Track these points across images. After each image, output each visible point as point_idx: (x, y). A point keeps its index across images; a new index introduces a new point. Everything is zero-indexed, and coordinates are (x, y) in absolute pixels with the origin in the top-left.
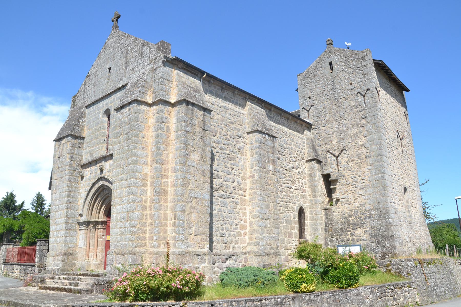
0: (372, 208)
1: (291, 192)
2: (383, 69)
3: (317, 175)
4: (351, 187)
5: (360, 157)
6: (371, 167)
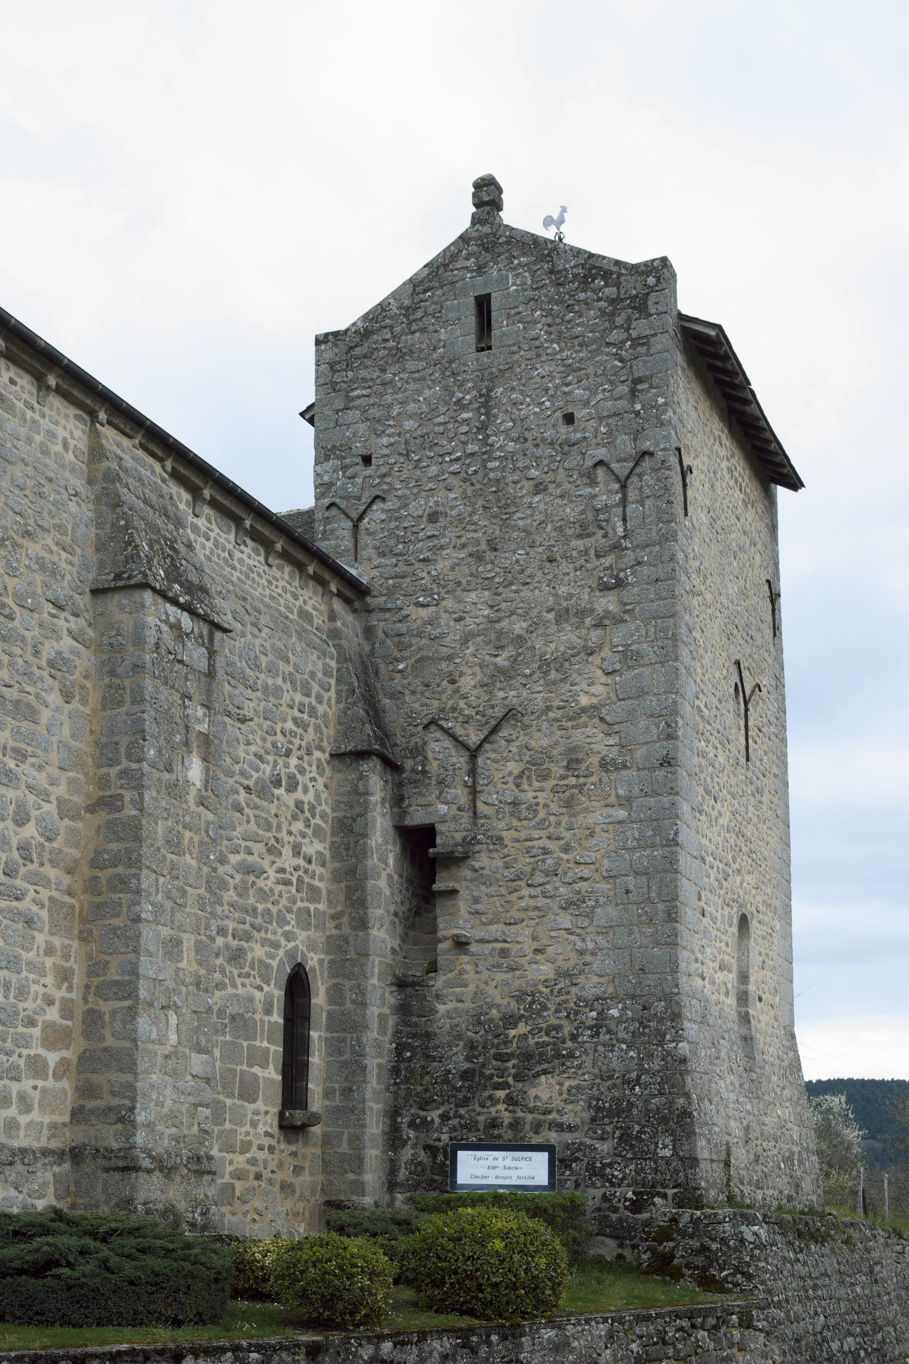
0: (611, 990)
1: (263, 895)
2: (712, 368)
3: (378, 825)
4: (525, 892)
5: (578, 761)
6: (622, 814)
